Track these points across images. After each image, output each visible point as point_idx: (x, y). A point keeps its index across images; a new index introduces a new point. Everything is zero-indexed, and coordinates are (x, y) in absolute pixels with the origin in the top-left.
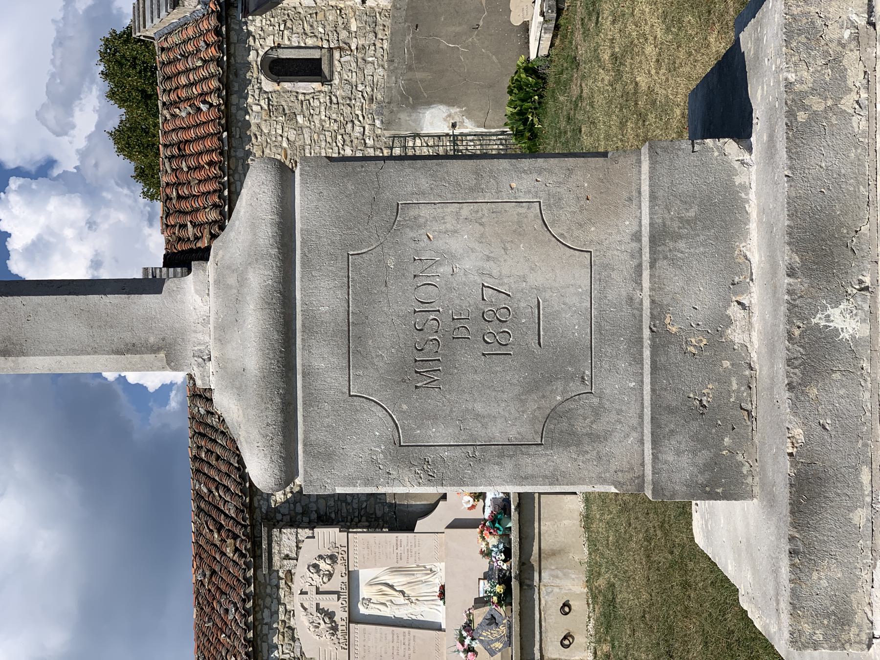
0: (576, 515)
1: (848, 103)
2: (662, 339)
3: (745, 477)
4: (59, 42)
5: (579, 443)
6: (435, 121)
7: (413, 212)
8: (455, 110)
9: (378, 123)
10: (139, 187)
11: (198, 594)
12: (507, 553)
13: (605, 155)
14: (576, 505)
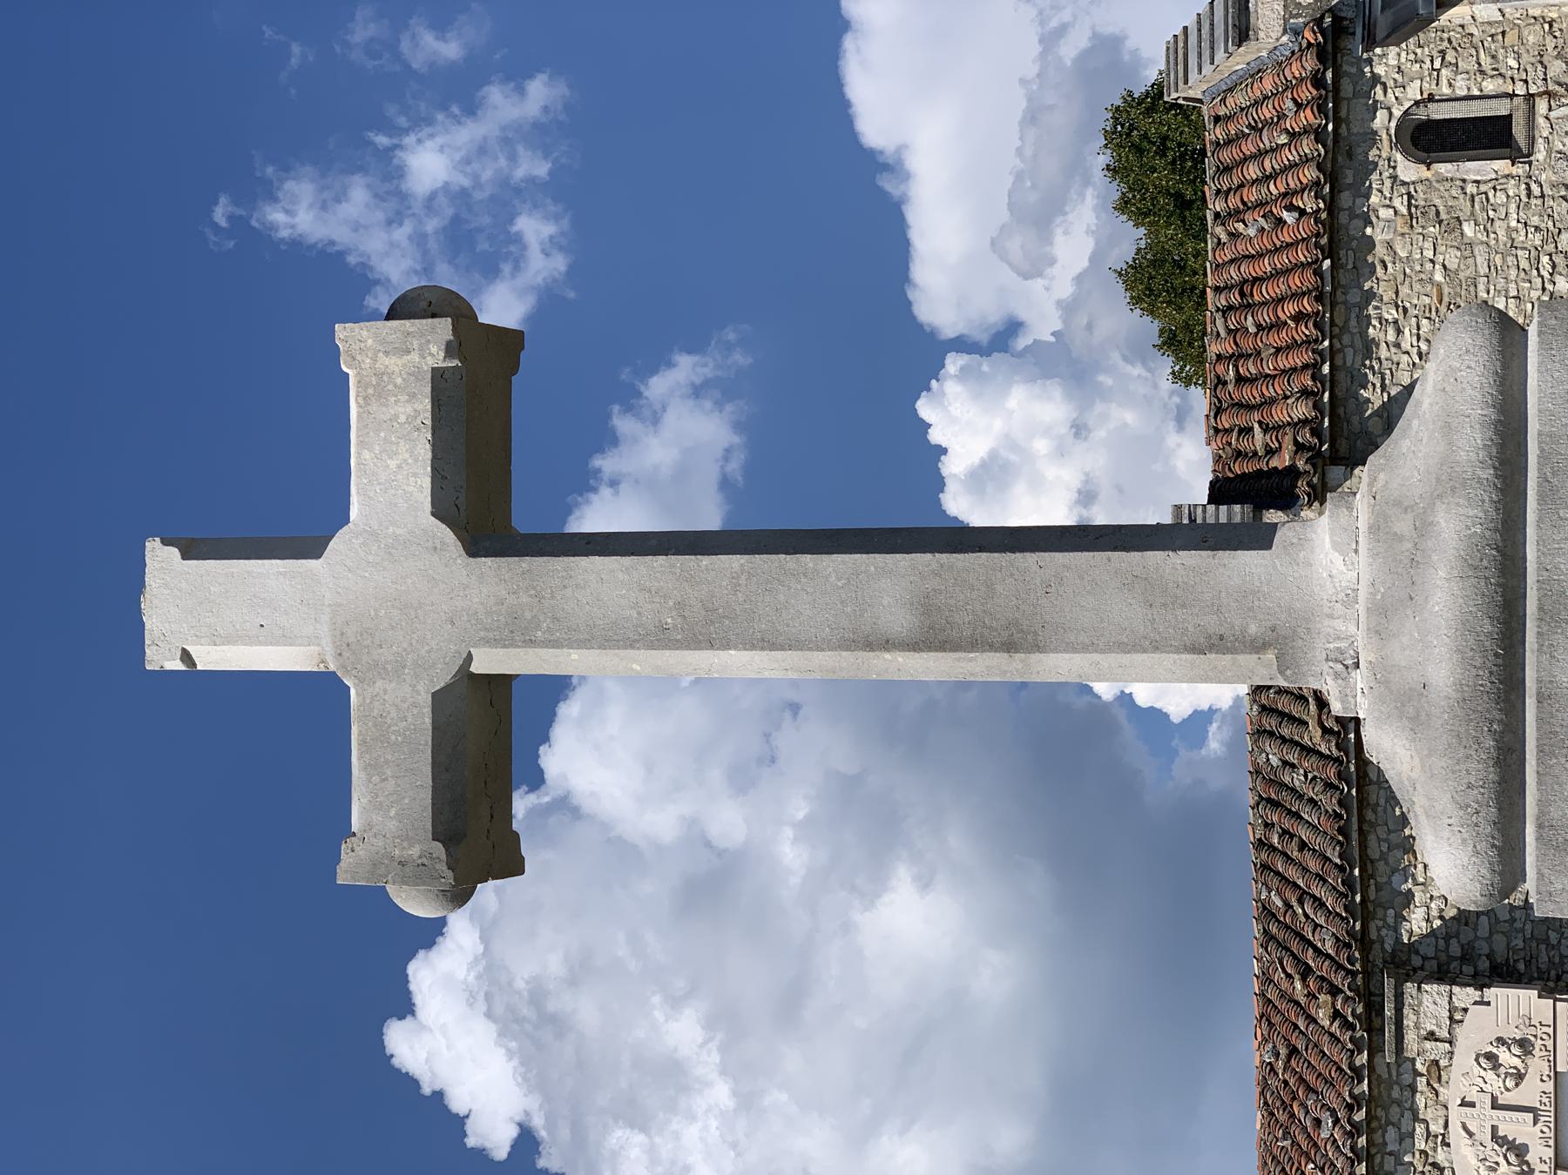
4: (1031, 117)
10: (1166, 364)
11: (1264, 1087)
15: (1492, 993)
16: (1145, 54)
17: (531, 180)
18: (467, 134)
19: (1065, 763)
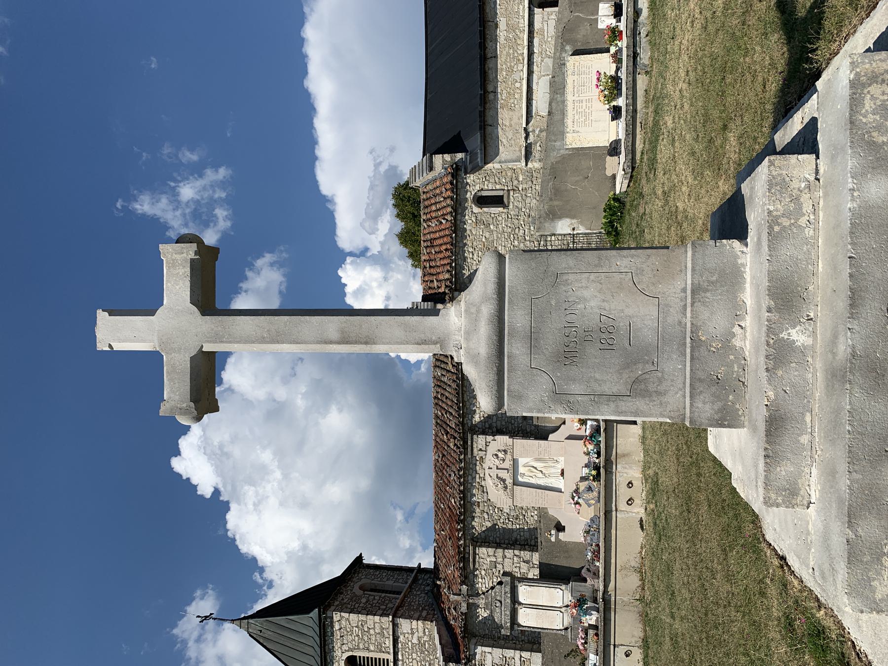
0: (637, 436)
1: (803, 221)
2: (696, 343)
3: (740, 416)
4: (372, 188)
5: (651, 396)
6: (563, 227)
7: (565, 277)
8: (574, 221)
9: (532, 228)
10: (410, 262)
11: (436, 465)
12: (599, 454)
13: (668, 248)
14: (636, 430)
15: (496, 437)
16: (404, 172)
17: (220, 198)
18: (199, 183)
19: (382, 375)
